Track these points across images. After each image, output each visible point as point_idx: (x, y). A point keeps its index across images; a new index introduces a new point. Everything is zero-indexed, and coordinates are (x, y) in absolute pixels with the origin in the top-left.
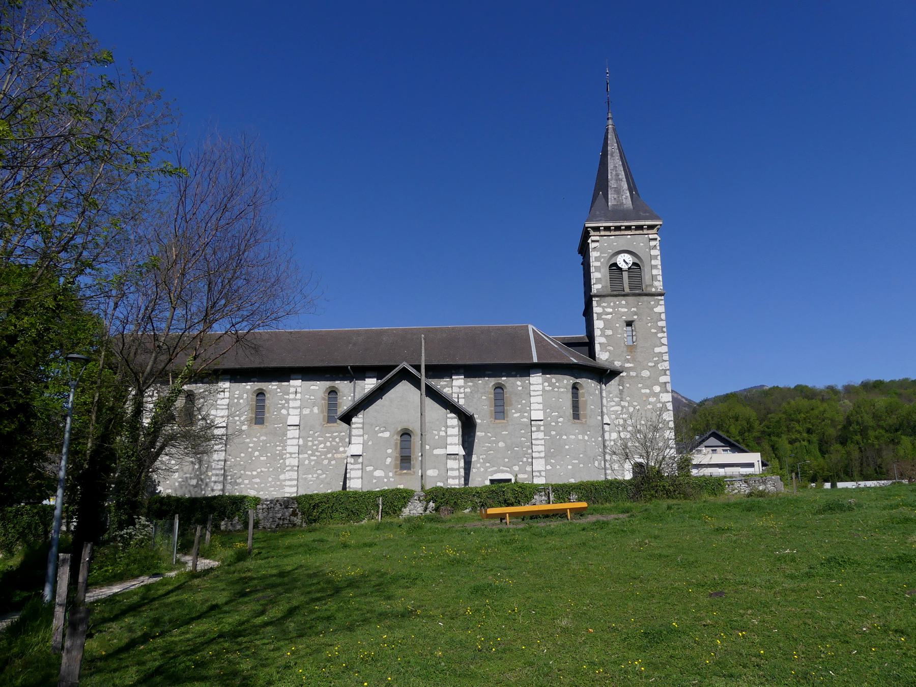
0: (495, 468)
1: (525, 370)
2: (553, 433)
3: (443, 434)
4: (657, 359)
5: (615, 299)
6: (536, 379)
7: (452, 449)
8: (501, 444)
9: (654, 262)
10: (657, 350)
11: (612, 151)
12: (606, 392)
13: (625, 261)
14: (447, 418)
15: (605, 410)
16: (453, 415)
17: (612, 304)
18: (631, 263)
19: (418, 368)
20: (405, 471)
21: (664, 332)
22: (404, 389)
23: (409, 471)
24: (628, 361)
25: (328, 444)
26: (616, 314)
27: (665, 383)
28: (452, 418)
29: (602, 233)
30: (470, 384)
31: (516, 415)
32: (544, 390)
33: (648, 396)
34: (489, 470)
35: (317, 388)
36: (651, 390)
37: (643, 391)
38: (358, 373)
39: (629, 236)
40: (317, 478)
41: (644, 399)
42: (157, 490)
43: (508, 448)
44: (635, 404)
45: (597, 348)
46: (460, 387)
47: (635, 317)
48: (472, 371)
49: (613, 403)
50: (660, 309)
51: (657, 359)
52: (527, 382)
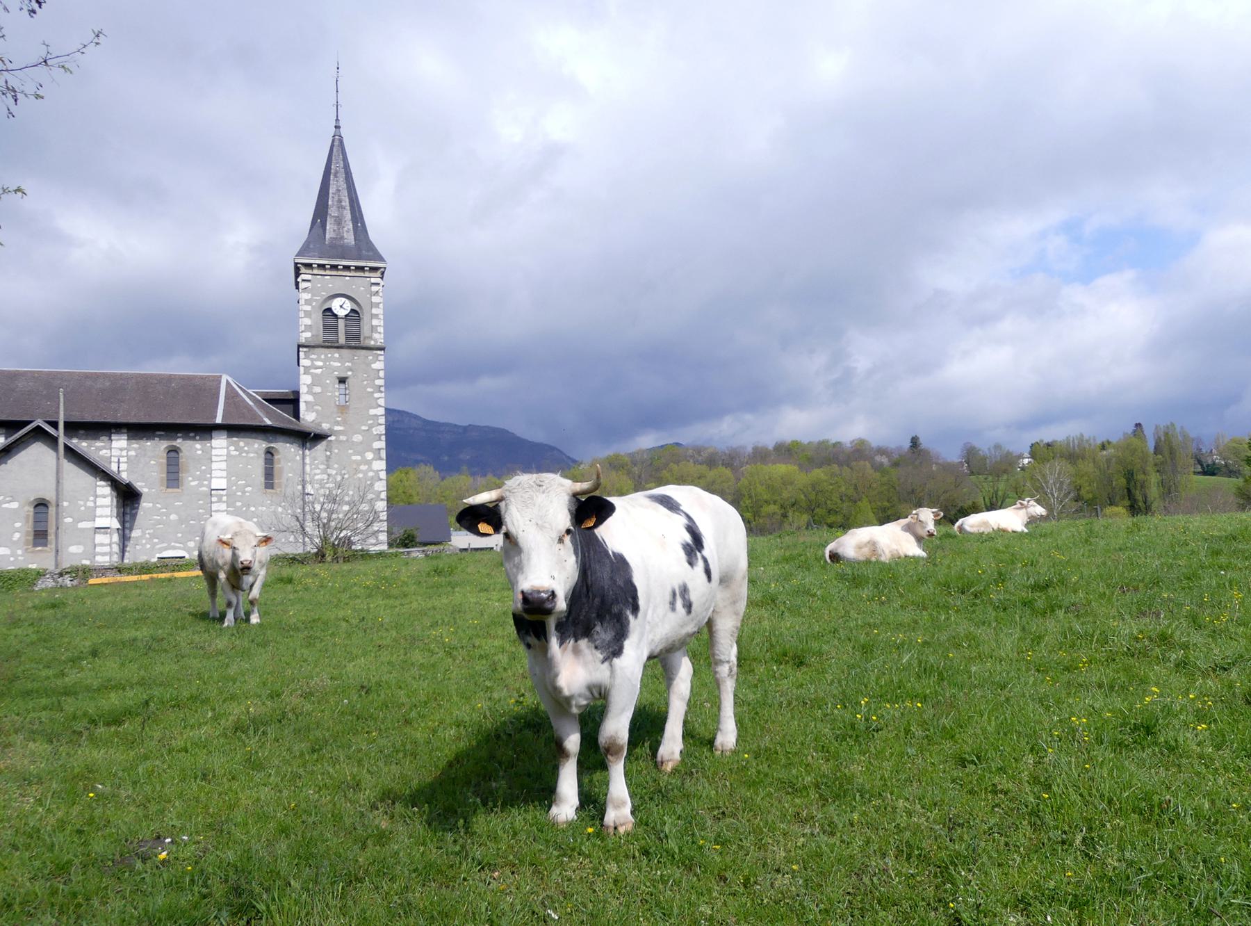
0: (165, 545)
1: (205, 430)
2: (239, 504)
3: (90, 504)
4: (371, 422)
5: (327, 351)
6: (220, 443)
7: (100, 522)
8: (173, 517)
9: (374, 311)
10: (372, 412)
11: (336, 170)
12: (310, 458)
13: (341, 307)
14: (97, 486)
15: (308, 478)
16: (103, 483)
17: (323, 357)
18: (349, 310)
19: (54, 425)
20: (39, 548)
21: (382, 392)
22: (37, 452)
23: (45, 548)
24: (338, 424)
26: (327, 368)
27: (379, 449)
28: (103, 486)
29: (315, 272)
30: (135, 446)
31: (193, 484)
32: (228, 455)
33: (359, 463)
34: (158, 546)
36: (363, 456)
37: (354, 458)
39: (348, 278)
43: (181, 521)
45: (302, 406)
46: (121, 450)
47: (350, 373)
48: (139, 430)
49: (318, 471)
50: (379, 366)
51: (371, 422)
52: (209, 445)
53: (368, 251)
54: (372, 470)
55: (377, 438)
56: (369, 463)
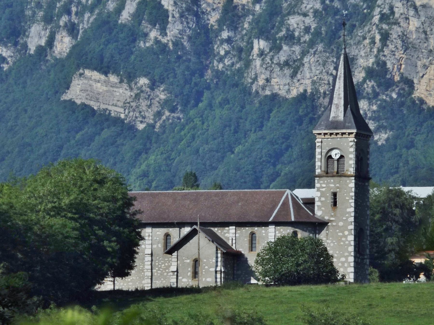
1: (266, 224)
17: (326, 182)
24: (332, 216)
25: (166, 264)
28: (110, 285)
33: (342, 237)
35: (160, 233)
38: (181, 225)
40: (162, 282)
41: (339, 238)
42: (383, 130)
44: (334, 241)
47: (338, 190)
48: (239, 224)
53: (349, 123)
54: (347, 241)
55: (350, 223)
56: (346, 237)
